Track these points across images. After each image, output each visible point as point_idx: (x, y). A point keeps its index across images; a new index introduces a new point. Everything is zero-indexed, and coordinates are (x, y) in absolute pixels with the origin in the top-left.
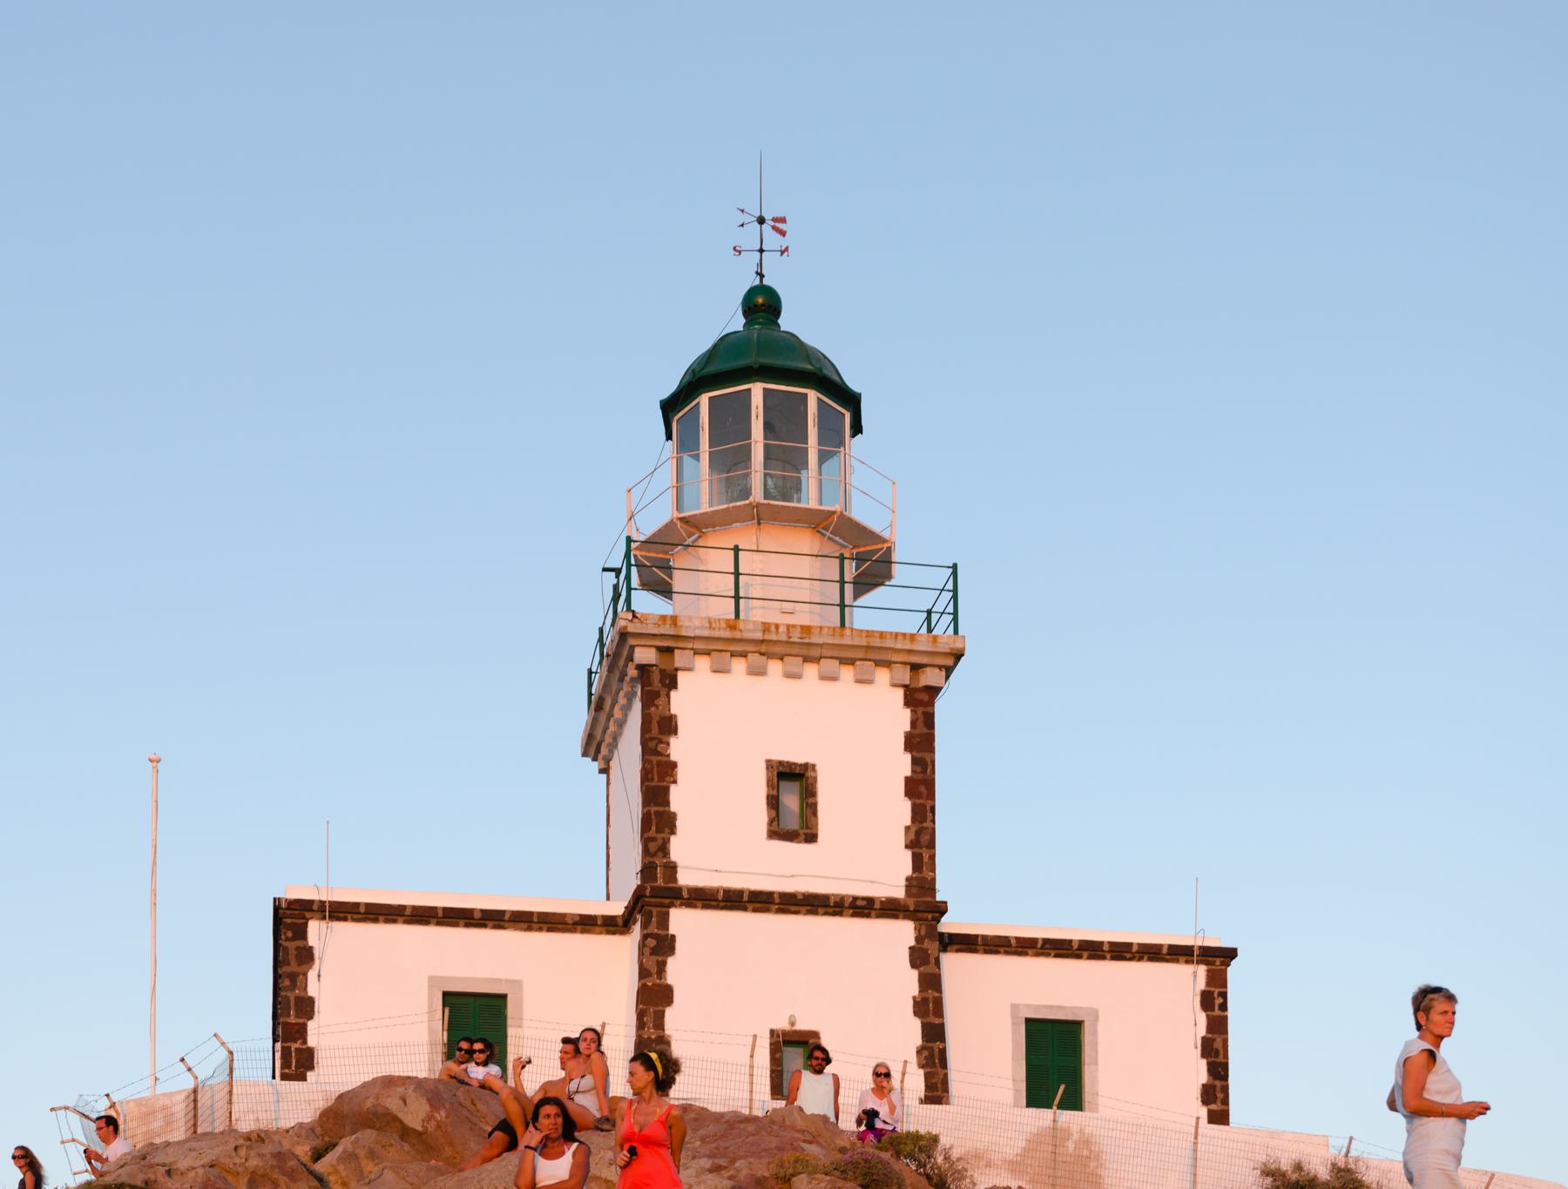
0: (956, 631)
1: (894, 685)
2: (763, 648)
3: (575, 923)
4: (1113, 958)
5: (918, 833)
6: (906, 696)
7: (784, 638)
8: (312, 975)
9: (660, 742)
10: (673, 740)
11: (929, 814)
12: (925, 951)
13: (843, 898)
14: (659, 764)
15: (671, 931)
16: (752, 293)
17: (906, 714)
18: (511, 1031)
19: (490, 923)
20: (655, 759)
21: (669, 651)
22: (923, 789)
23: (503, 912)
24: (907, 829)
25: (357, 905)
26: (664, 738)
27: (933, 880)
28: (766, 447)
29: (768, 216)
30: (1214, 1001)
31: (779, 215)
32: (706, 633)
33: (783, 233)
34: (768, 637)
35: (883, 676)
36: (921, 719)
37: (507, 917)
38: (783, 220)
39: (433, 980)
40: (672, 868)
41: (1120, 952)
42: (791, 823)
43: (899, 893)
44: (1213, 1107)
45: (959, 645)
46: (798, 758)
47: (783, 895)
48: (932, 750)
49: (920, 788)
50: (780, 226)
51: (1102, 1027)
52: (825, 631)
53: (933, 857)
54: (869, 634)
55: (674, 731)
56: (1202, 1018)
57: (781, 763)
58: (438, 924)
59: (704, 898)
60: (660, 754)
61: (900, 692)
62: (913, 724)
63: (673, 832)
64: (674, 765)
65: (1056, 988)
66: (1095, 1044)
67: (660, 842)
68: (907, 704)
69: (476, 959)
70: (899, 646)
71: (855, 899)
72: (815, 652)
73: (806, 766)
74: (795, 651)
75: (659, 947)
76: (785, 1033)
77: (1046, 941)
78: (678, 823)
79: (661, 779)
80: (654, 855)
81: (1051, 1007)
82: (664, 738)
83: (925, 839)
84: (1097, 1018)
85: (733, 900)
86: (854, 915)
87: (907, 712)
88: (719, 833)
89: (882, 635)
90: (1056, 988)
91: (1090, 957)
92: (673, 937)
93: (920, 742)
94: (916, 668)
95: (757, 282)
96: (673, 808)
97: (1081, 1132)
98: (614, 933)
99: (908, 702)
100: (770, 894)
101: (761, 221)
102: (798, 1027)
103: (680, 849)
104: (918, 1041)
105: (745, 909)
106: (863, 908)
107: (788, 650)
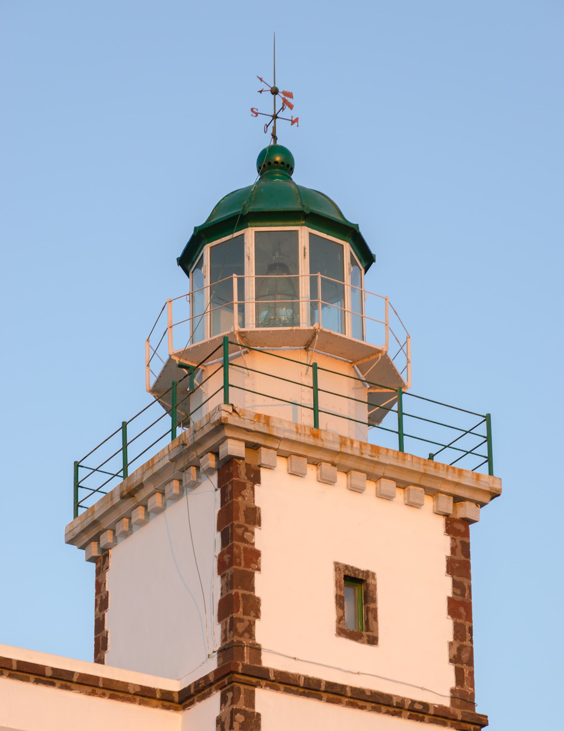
0: (491, 472)
1: (437, 513)
2: (337, 460)
3: (136, 694)
5: (460, 649)
6: (447, 524)
7: (357, 453)
9: (246, 530)
11: (468, 634)
14: (245, 549)
17: (447, 540)
19: (58, 683)
22: (462, 610)
26: (250, 527)
27: (473, 695)
29: (280, 90)
31: (288, 90)
32: (294, 437)
34: (344, 450)
35: (428, 503)
36: (459, 548)
37: (75, 679)
40: (257, 650)
42: (350, 625)
43: (446, 703)
45: (496, 486)
46: (361, 564)
48: (469, 577)
49: (460, 607)
52: (391, 453)
53: (472, 674)
55: (257, 521)
57: (346, 567)
58: (11, 676)
59: (287, 683)
60: (247, 542)
62: (453, 550)
63: (257, 616)
64: (257, 554)
67: (247, 623)
70: (450, 478)
71: (413, 702)
72: (379, 471)
73: (367, 572)
78: (262, 608)
79: (247, 565)
80: (241, 635)
82: (250, 527)
83: (465, 656)
85: (311, 688)
86: (410, 718)
92: (259, 715)
93: (459, 566)
94: (457, 499)
96: (257, 594)
98: (168, 708)
101: (275, 92)
103: (264, 632)
105: (320, 698)
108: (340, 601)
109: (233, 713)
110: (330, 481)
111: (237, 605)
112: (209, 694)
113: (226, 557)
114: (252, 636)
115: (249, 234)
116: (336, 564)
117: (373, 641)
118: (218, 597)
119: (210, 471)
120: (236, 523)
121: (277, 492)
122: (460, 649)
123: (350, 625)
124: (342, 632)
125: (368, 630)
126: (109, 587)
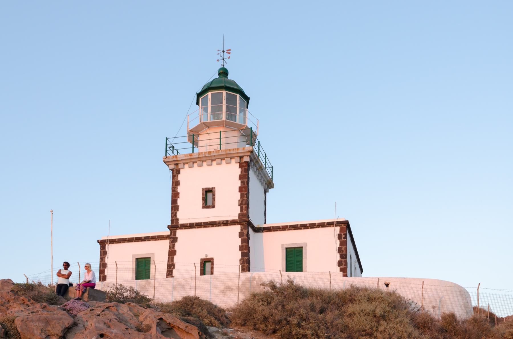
1: (236, 163)
2: (200, 159)
4: (311, 228)
5: (242, 201)
8: (106, 258)
10: (179, 187)
12: (243, 233)
13: (220, 221)
16: (221, 69)
21: (177, 165)
23: (149, 237)
24: (239, 200)
25: (116, 239)
30: (112, 241)
31: (228, 49)
32: (184, 158)
33: (229, 53)
38: (230, 50)
39: (153, 254)
40: (177, 220)
41: (313, 226)
43: (236, 218)
44: (341, 267)
46: (210, 186)
47: (204, 223)
50: (229, 52)
51: (308, 248)
54: (226, 150)
56: (338, 242)
57: (206, 188)
58: (135, 241)
61: (238, 164)
63: (178, 210)
64: (179, 193)
65: (293, 238)
66: (306, 253)
68: (240, 167)
71: (223, 221)
72: (213, 158)
73: (213, 188)
74: (208, 159)
75: (173, 239)
76: (204, 259)
77: (290, 226)
79: (175, 197)
81: (293, 244)
84: (306, 245)
85: (192, 226)
87: (240, 169)
88: (191, 210)
89: (229, 150)
90: (293, 238)
91: (304, 229)
96: (178, 204)
97: (259, 278)
100: (201, 223)
101: (223, 52)
102: (208, 257)
103: (179, 215)
104: (240, 257)
106: (226, 223)
107: (206, 159)
110: (201, 166)
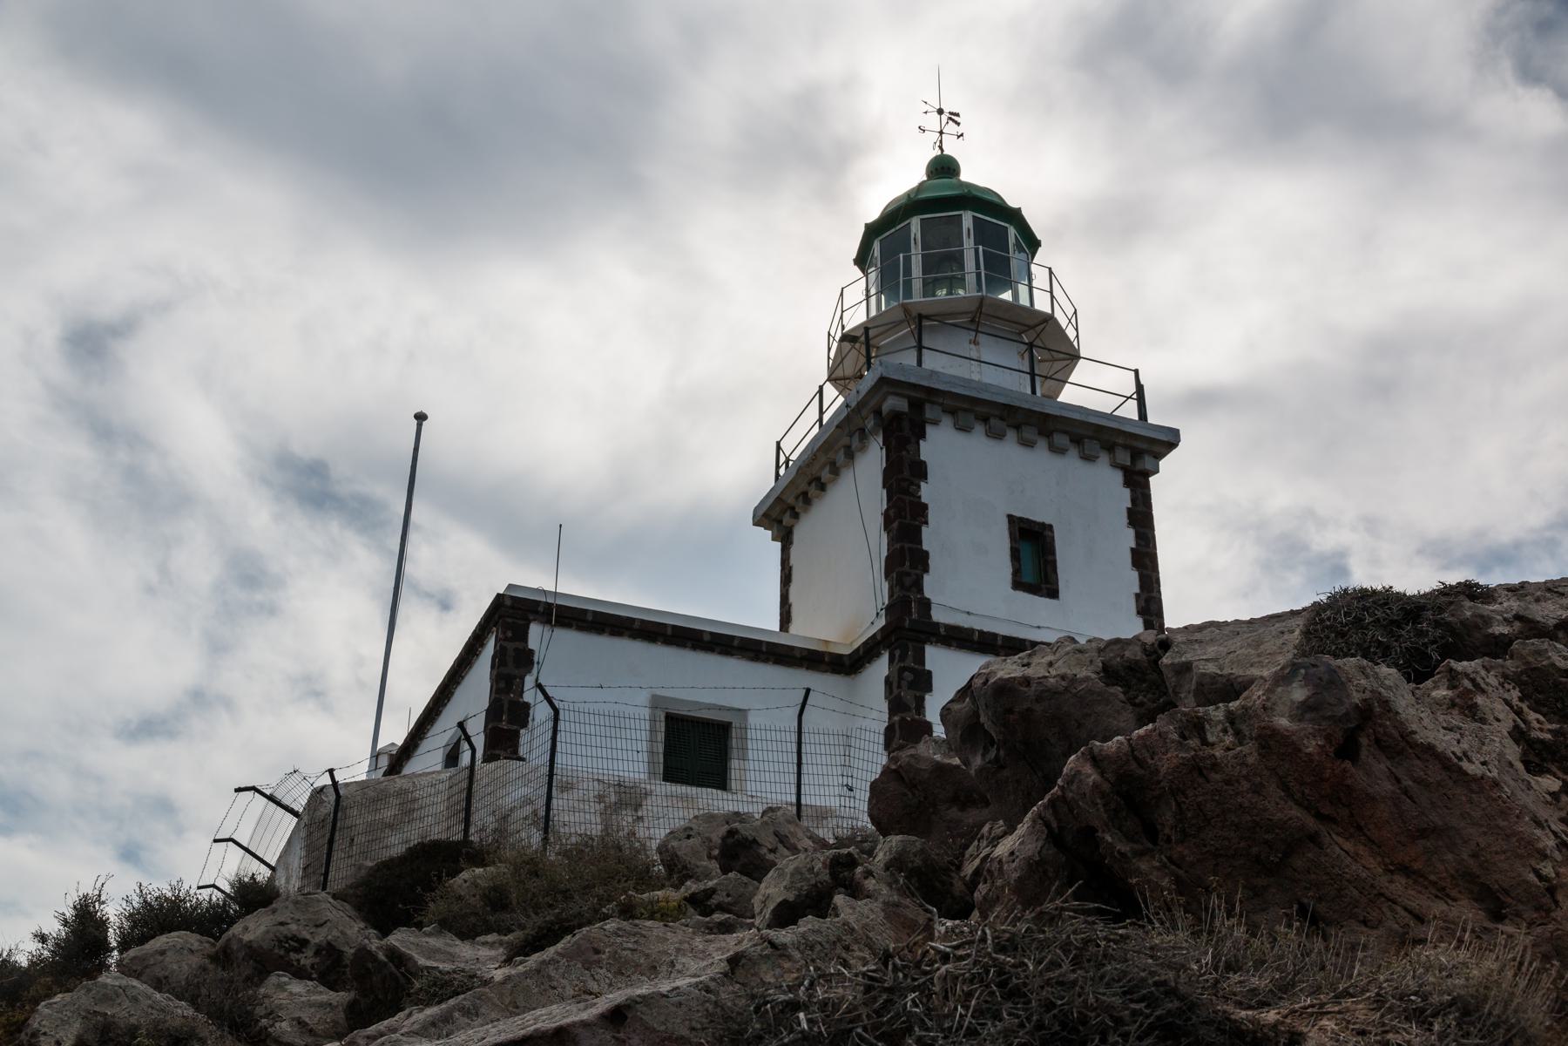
15: (928, 667)
18: (734, 764)
20: (907, 498)
28: (962, 267)
29: (946, 110)
40: (926, 605)
42: (1028, 577)
46: (1038, 514)
55: (924, 477)
57: (1021, 519)
62: (1133, 501)
64: (925, 507)
69: (705, 684)
92: (930, 673)
95: (938, 152)
99: (1127, 483)
101: (940, 112)
103: (931, 586)
108: (1015, 555)
109: (902, 670)
111: (906, 560)
112: (878, 655)
113: (891, 513)
114: (920, 590)
115: (915, 224)
116: (1010, 517)
117: (1053, 593)
118: (885, 554)
119: (873, 433)
120: (904, 478)
121: (942, 446)
122: (1148, 601)
123: (1028, 577)
124: (1018, 584)
125: (1047, 582)
126: (792, 562)
